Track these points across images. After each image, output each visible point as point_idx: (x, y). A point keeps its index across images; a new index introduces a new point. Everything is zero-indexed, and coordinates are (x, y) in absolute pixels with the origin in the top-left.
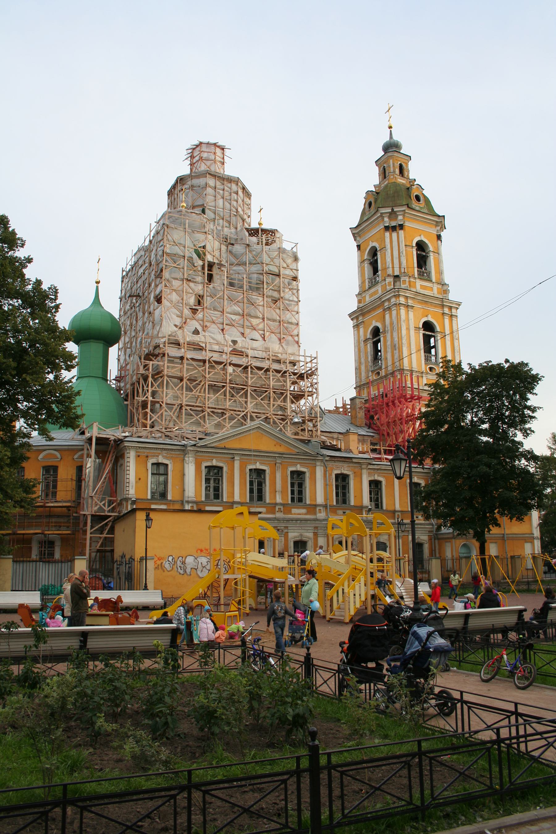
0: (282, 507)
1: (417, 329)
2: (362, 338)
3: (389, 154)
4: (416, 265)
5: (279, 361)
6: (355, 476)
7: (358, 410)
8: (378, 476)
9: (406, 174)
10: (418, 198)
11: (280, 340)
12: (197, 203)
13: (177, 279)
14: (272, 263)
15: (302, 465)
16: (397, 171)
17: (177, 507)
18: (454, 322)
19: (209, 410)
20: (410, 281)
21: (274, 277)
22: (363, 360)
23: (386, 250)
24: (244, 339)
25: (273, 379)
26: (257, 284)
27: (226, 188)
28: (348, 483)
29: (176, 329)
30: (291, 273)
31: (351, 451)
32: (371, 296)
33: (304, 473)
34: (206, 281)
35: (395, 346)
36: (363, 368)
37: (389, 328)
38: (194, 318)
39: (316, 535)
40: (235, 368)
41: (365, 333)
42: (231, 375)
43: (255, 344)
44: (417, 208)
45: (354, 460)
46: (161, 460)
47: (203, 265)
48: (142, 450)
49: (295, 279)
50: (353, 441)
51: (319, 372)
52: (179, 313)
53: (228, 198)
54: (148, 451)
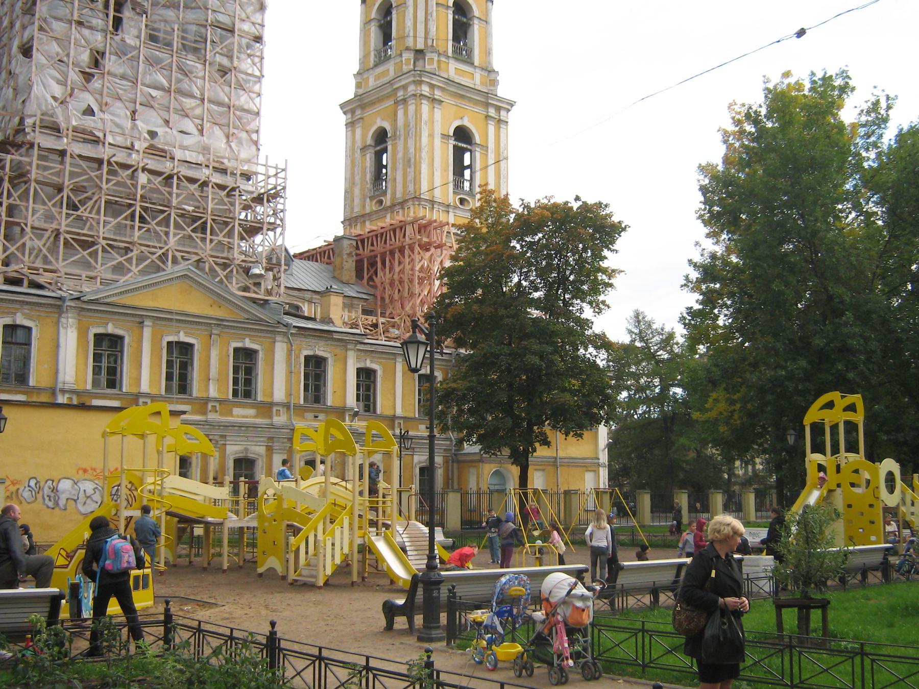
0: (217, 405)
1: (445, 136)
2: (359, 144)
5: (224, 171)
7: (345, 257)
11: (228, 137)
14: (222, 10)
17: (44, 398)
18: (502, 131)
19: (104, 242)
20: (439, 61)
21: (224, 33)
22: (357, 179)
25: (213, 199)
26: (196, 41)
28: (324, 371)
30: (253, 30)
32: (377, 78)
34: (111, 28)
35: (409, 160)
36: (357, 191)
37: (402, 132)
40: (151, 177)
41: (364, 136)
42: (143, 187)
43: (188, 141)
46: (20, 320)
49: (258, 39)
50: (336, 305)
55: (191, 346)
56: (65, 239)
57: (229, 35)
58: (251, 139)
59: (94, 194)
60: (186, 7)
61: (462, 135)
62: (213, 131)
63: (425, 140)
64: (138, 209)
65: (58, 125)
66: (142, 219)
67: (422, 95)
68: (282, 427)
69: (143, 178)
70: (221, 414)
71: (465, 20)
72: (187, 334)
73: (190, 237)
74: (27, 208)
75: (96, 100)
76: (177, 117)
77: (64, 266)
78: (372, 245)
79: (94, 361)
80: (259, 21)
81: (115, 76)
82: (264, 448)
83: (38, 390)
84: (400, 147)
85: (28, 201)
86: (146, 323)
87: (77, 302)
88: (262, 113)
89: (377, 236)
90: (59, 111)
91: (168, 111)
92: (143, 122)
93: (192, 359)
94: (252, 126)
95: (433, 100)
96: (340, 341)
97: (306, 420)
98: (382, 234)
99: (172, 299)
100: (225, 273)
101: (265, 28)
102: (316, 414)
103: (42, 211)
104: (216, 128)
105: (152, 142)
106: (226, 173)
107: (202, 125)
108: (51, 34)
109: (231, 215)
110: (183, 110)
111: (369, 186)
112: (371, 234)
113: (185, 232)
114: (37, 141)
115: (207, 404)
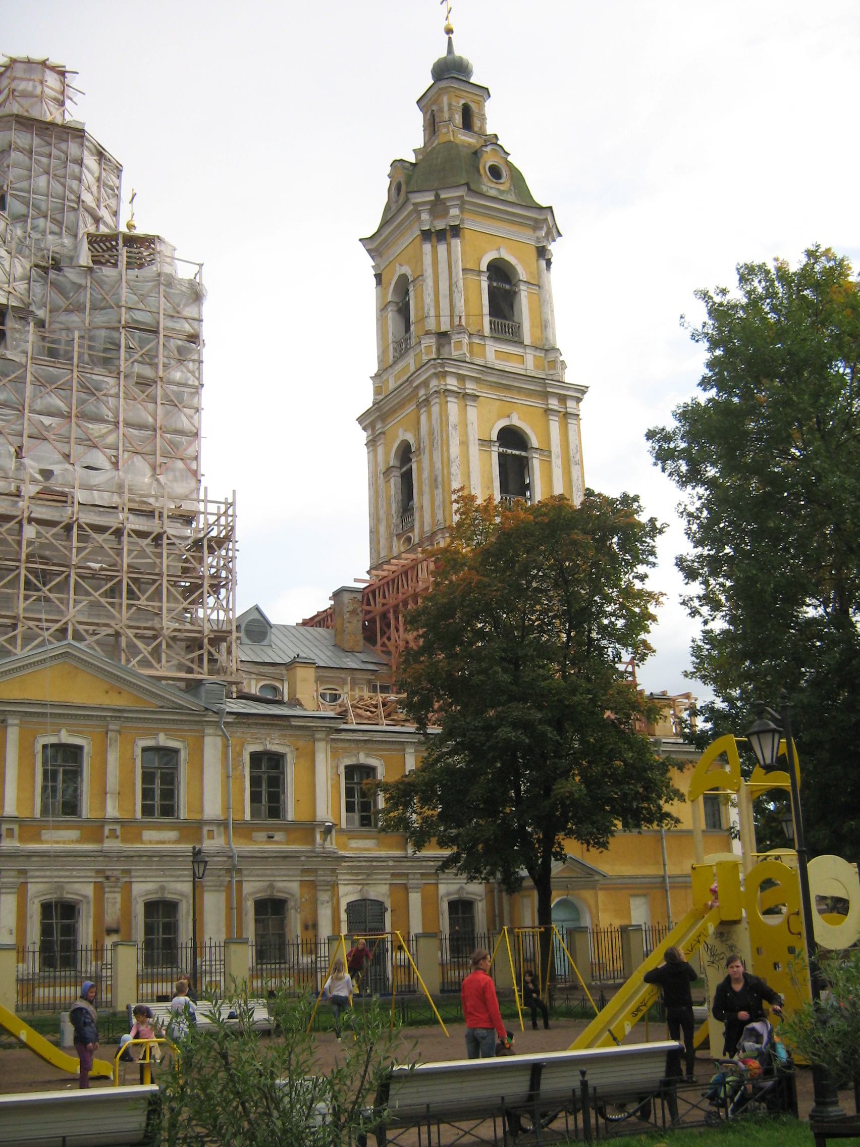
0: (118, 827)
1: (485, 443)
2: (382, 468)
3: (443, 84)
4: (486, 310)
5: (150, 514)
6: (297, 757)
7: (347, 616)
8: (367, 755)
9: (477, 124)
10: (495, 172)
11: (154, 468)
15: (169, 734)
16: (458, 119)
18: (572, 428)
20: (471, 344)
21: (145, 335)
22: (382, 513)
23: (423, 281)
25: (130, 552)
26: (106, 350)
27: (55, 152)
28: (283, 773)
30: (187, 328)
31: (295, 702)
32: (397, 377)
33: (176, 751)
35: (436, 480)
36: (382, 528)
37: (427, 443)
39: (100, 889)
40: (42, 529)
41: (387, 454)
42: (30, 543)
43: (97, 478)
44: (493, 193)
45: (295, 722)
49: (194, 338)
50: (304, 680)
51: (239, 534)
53: (60, 172)
55: (80, 748)
57: (152, 336)
58: (189, 469)
60: (94, 308)
61: (511, 437)
62: (133, 463)
63: (455, 450)
64: (23, 572)
66: (131, 594)
67: (466, 394)
68: (217, 854)
69: (30, 532)
70: (124, 840)
71: (507, 287)
72: (71, 733)
73: (47, 600)
76: (81, 449)
78: (384, 597)
79: (144, 782)
82: (92, 886)
84: (426, 464)
85: (161, 600)
86: (10, 721)
88: (203, 433)
89: (388, 583)
91: (68, 443)
92: (33, 459)
93: (81, 766)
94: (191, 451)
95: (464, 396)
96: (307, 730)
97: (256, 842)
98: (393, 580)
99: (48, 687)
100: (150, 648)
101: (204, 323)
103: (84, 603)
104: (138, 459)
105: (47, 484)
106: (154, 516)
107: (116, 457)
109: (157, 571)
110: (90, 440)
111: (395, 520)
112: (382, 582)
113: (91, 598)
115: (102, 827)
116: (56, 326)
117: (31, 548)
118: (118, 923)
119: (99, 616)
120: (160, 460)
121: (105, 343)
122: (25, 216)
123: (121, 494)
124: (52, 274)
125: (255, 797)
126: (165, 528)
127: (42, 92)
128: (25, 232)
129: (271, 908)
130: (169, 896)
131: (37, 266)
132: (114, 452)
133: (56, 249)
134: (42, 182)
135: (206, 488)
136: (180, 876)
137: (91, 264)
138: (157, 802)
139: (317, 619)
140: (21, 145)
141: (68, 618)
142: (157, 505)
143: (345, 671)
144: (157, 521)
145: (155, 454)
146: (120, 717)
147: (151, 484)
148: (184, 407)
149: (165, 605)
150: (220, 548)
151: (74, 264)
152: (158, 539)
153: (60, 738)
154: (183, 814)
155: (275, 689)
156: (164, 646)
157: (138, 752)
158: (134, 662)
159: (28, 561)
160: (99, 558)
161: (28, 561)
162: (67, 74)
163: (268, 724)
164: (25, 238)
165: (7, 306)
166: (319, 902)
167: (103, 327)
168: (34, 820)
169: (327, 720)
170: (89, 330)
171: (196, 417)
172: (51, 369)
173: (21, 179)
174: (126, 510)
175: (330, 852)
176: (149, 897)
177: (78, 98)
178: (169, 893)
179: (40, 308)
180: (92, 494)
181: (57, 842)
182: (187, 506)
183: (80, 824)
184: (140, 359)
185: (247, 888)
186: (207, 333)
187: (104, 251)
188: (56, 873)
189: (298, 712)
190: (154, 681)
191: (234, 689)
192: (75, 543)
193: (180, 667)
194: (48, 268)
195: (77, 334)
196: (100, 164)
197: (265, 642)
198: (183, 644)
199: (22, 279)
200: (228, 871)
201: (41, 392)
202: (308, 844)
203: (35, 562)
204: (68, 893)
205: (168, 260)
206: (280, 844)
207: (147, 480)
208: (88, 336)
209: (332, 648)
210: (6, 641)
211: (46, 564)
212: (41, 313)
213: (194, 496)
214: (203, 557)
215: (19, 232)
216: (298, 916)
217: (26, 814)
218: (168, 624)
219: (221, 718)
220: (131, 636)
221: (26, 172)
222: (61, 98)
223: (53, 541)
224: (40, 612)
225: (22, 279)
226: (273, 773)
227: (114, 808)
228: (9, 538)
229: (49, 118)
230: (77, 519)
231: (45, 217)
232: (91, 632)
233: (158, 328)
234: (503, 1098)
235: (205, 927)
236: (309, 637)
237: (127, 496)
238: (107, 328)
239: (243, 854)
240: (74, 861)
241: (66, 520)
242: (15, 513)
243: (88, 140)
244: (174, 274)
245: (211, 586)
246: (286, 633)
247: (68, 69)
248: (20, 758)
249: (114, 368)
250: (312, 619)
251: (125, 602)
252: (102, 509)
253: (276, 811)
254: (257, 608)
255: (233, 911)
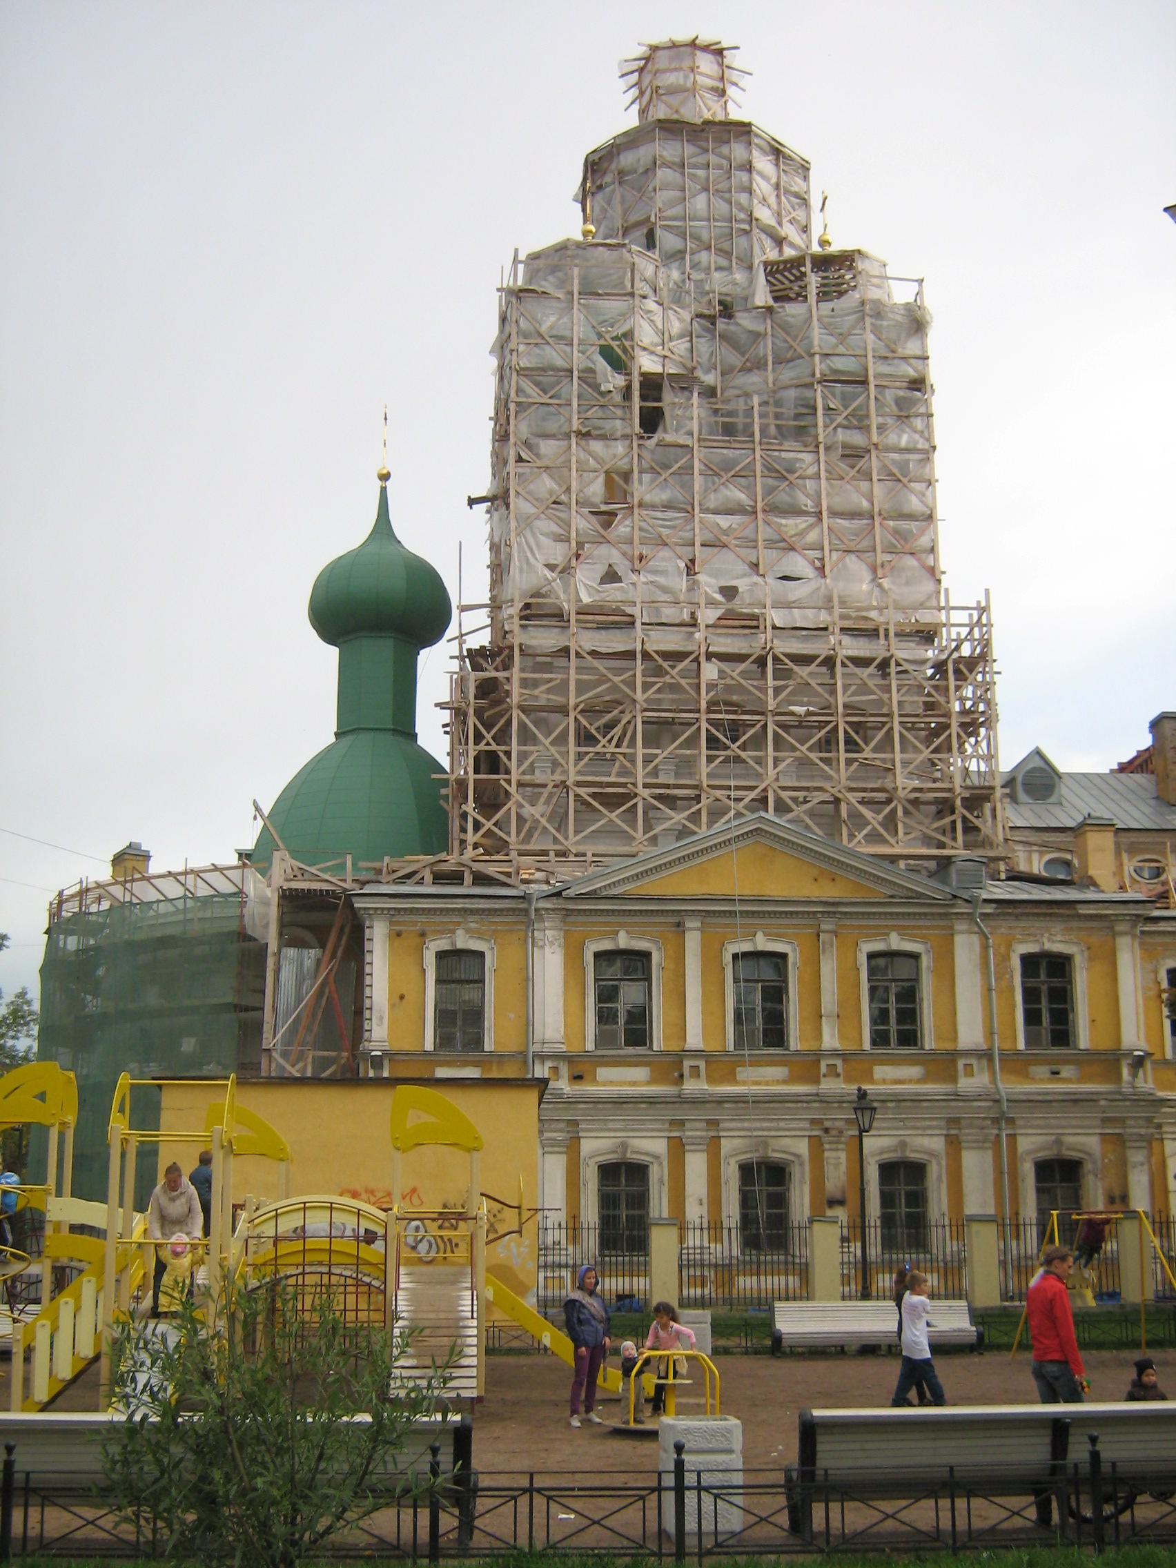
0: (838, 1062)
5: (873, 633)
6: (1090, 959)
11: (874, 570)
12: (633, 218)
13: (552, 436)
14: (841, 349)
15: (903, 932)
17: (510, 1072)
19: (646, 793)
21: (849, 389)
24: (756, 579)
25: (846, 687)
26: (798, 416)
27: (713, 159)
28: (1070, 982)
29: (549, 575)
31: (1092, 883)
33: (647, 955)
34: (637, 429)
38: (603, 541)
39: (817, 1146)
40: (724, 666)
42: (711, 686)
43: (796, 591)
45: (1083, 910)
46: (463, 941)
47: (629, 387)
48: (407, 918)
49: (919, 384)
51: (997, 651)
52: (556, 529)
53: (723, 186)
54: (423, 918)
56: (577, 795)
57: (860, 389)
59: (622, 712)
60: (778, 361)
65: (561, 609)
66: (851, 745)
68: (979, 1097)
69: (710, 671)
73: (738, 760)
74: (508, 754)
75: (624, 554)
76: (774, 554)
77: (577, 843)
80: (918, 352)
81: (653, 507)
83: (499, 1058)
85: (893, 751)
86: (688, 924)
87: (554, 900)
88: (940, 513)
90: (558, 586)
91: (756, 547)
92: (710, 575)
94: (924, 541)
96: (1104, 920)
97: (1034, 1080)
99: (736, 877)
102: (1055, 1068)
103: (789, 761)
104: (851, 560)
105: (730, 606)
106: (878, 636)
107: (822, 560)
108: (539, 464)
109: (885, 710)
110: (784, 540)
113: (797, 754)
114: (516, 643)
115: (819, 1061)
116: (731, 393)
117: (712, 693)
118: (844, 1193)
119: (812, 777)
120: (881, 557)
121: (796, 407)
122: (683, 252)
123: (830, 609)
124: (721, 324)
125: (1032, 1018)
126: (893, 651)
127: (695, 82)
128: (683, 273)
129: (1059, 1173)
130: (912, 1155)
131: (699, 316)
132: (817, 554)
133: (724, 290)
134: (700, 202)
135: (947, 590)
136: (924, 1128)
137: (771, 302)
138: (893, 1027)
139: (1137, 762)
140: (668, 158)
141: (767, 782)
142: (882, 619)
143: (1167, 834)
144: (882, 641)
145: (874, 550)
146: (835, 913)
147: (871, 592)
148: (910, 481)
149: (898, 756)
150: (971, 671)
151: (749, 305)
152: (884, 665)
153: (755, 944)
154: (929, 1042)
155: (1068, 864)
156: (900, 813)
157: (863, 959)
158: (860, 837)
159: (709, 711)
160: (805, 699)
161: (709, 711)
162: (725, 53)
163: (1045, 915)
164: (684, 281)
165: (661, 374)
166: (1129, 1166)
167: (791, 386)
168: (727, 1054)
169: (1131, 906)
170: (775, 392)
171: (928, 493)
172: (725, 451)
173: (672, 204)
174: (837, 631)
175: (1143, 1094)
176: (885, 1156)
177: (744, 81)
178: (912, 1151)
179: (707, 372)
180: (791, 613)
181: (757, 1083)
182: (926, 617)
183: (788, 1058)
184: (845, 422)
185: (1025, 1144)
186: (936, 374)
187: (791, 281)
188: (758, 1125)
189: (1091, 895)
190: (886, 864)
191: (1002, 867)
192: (770, 682)
193: (927, 840)
194: (714, 317)
195: (756, 400)
196: (777, 165)
197: (1053, 799)
198: (933, 808)
199: (681, 336)
200: (996, 1120)
201: (714, 483)
202: (943, 1080)
203: (720, 712)
204: (773, 1151)
205: (875, 281)
206: (1070, 1083)
207: (864, 587)
208: (773, 400)
209: (1153, 802)
210: (687, 819)
211: (735, 712)
212: (709, 379)
213: (934, 603)
214: (950, 685)
215: (675, 275)
216: (1099, 1184)
217: (713, 1046)
218: (904, 783)
219: (975, 907)
220: (853, 801)
221: (678, 194)
222: (721, 86)
223: (742, 681)
224: (728, 777)
225: (681, 336)
226: (1056, 982)
227: (833, 1035)
228: (683, 682)
229: (707, 115)
230: (771, 648)
231: (709, 248)
232: (801, 799)
233: (867, 376)
234: (951, 1468)
235: (965, 1199)
236: (1120, 788)
237: (837, 611)
238: (797, 386)
239: (1017, 1097)
240: (931, 1107)
241: (758, 652)
242: (689, 649)
243: (757, 135)
244: (885, 298)
245: (963, 725)
246: (1104, 786)
247: (724, 45)
248: (704, 973)
249: (810, 439)
250: (1131, 762)
251: (843, 755)
252: (804, 633)
253: (1062, 1035)
254: (1038, 753)
255: (1005, 1177)
